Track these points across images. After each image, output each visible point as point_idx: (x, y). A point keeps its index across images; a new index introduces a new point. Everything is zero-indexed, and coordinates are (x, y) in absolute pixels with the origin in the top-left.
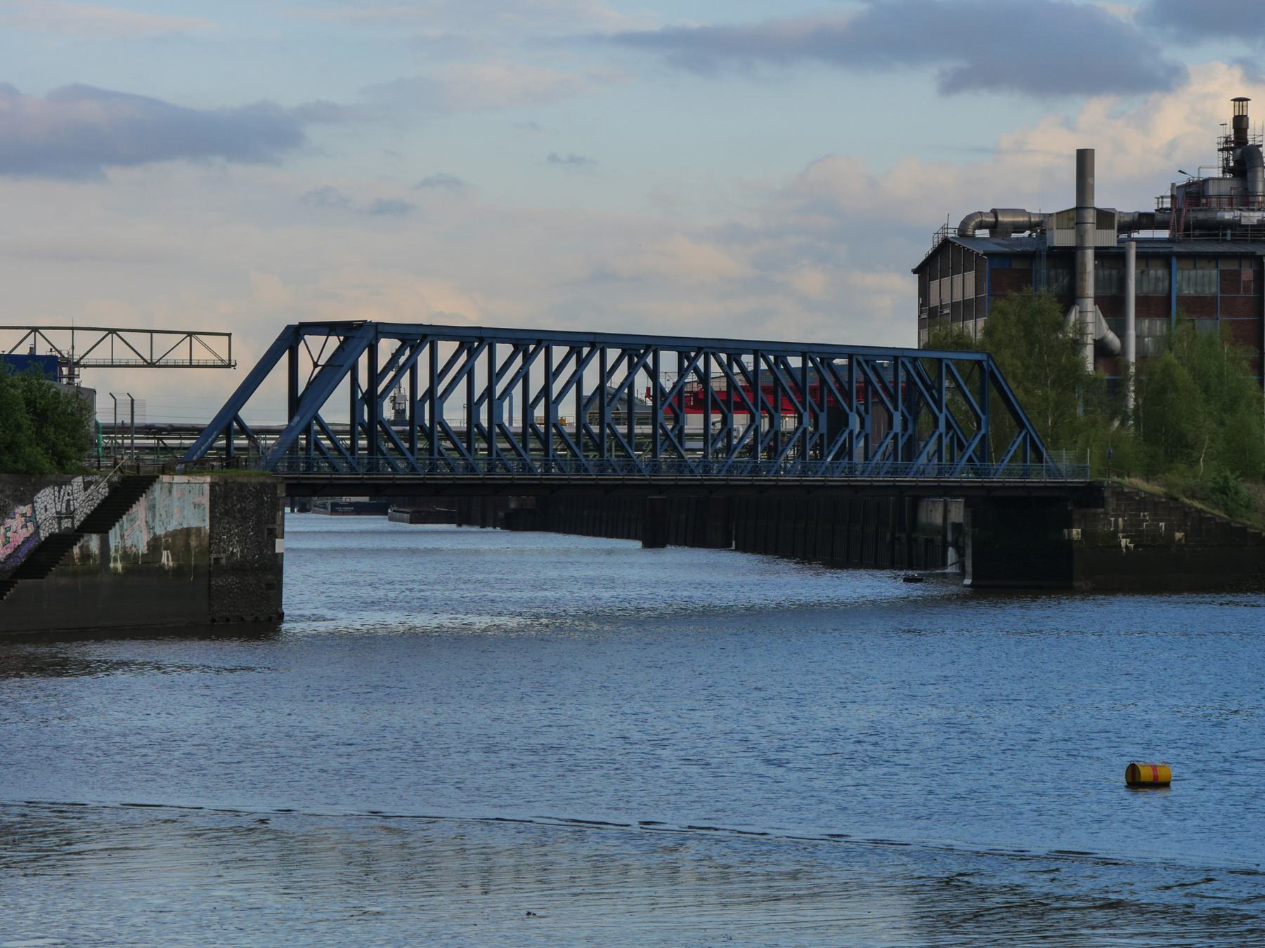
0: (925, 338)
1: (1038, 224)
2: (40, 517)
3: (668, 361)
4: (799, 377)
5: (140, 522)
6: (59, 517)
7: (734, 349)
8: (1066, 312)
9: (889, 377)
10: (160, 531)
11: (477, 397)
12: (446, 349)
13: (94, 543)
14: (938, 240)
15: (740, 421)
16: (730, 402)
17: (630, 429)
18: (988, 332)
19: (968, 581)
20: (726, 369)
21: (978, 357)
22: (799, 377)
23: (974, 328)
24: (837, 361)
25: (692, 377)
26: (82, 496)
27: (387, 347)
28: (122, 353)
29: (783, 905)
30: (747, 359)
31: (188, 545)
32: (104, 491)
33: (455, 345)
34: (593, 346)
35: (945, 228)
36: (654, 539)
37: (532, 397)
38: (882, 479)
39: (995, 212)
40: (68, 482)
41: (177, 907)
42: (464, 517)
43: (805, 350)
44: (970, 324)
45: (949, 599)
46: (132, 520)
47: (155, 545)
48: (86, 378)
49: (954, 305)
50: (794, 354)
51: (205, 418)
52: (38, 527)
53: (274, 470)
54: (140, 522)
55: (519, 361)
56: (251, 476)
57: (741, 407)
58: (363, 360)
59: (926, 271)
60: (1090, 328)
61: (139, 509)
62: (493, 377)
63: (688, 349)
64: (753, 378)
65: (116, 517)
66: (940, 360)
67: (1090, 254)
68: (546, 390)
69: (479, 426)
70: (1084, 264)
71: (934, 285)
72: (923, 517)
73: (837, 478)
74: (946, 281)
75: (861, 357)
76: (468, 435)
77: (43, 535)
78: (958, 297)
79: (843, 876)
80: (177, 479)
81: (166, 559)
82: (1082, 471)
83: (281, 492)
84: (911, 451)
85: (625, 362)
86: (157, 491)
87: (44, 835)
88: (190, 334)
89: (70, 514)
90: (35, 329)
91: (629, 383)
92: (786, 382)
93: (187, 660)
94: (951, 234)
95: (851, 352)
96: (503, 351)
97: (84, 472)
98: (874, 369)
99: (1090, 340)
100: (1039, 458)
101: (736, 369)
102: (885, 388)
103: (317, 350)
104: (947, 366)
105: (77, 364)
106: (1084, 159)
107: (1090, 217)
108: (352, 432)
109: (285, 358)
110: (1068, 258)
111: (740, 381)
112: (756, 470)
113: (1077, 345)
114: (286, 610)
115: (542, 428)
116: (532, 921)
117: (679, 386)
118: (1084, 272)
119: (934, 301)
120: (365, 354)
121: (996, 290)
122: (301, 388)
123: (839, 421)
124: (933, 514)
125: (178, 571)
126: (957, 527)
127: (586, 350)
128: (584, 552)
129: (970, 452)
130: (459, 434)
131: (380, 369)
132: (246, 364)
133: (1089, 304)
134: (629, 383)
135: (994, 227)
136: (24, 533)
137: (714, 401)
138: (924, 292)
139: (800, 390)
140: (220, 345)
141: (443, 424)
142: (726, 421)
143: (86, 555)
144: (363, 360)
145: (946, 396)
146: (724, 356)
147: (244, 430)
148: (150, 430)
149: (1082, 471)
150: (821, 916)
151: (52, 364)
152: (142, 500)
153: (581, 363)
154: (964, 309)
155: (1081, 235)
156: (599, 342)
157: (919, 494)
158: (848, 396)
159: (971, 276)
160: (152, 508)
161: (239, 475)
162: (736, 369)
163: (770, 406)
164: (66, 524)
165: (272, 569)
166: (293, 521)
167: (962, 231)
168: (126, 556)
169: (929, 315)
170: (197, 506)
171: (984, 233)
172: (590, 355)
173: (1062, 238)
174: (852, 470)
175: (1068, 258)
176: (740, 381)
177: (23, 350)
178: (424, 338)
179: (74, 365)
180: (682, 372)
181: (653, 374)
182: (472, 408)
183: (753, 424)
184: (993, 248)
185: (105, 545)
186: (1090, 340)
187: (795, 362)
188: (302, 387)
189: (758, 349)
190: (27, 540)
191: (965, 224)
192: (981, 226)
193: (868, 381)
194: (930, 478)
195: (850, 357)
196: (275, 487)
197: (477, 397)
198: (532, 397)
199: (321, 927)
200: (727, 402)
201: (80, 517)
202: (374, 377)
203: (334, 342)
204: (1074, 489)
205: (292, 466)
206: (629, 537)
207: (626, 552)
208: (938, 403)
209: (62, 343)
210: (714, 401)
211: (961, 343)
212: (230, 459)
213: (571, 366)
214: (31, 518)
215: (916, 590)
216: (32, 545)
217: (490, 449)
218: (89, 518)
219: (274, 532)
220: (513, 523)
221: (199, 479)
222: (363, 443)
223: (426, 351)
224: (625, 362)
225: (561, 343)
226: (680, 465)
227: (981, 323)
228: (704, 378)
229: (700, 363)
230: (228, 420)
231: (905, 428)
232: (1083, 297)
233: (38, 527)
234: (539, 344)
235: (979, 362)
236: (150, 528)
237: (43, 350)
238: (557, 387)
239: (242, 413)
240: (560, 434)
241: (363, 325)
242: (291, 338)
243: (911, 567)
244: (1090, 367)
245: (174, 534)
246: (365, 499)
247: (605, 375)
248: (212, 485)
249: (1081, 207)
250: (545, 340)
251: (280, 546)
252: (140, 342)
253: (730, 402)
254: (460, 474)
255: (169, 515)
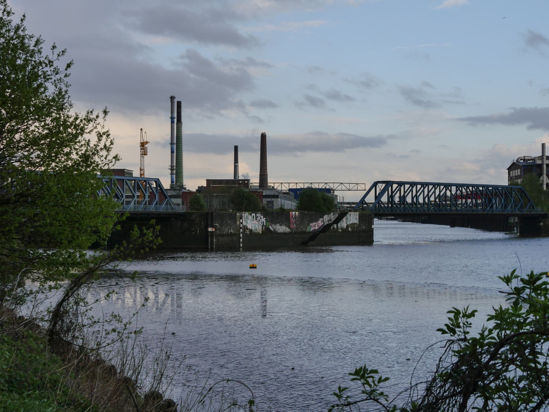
0: (509, 183)
1: (534, 159)
2: (325, 221)
3: (454, 188)
4: (491, 191)
5: (345, 222)
6: (328, 220)
7: (468, 186)
8: (540, 177)
9: (501, 191)
10: (348, 224)
11: (413, 196)
12: (407, 186)
13: (335, 226)
14: (512, 163)
15: (469, 201)
16: (467, 197)
17: (446, 203)
18: (523, 182)
19: (518, 234)
20: (466, 190)
21: (520, 187)
22: (491, 191)
23: (519, 181)
24: (490, 188)
25: (459, 192)
26: (333, 217)
27: (395, 186)
28: (344, 188)
29: (469, 300)
30: (471, 188)
31: (354, 226)
32: (337, 215)
33: (409, 185)
34: (438, 186)
35: (514, 160)
36: (453, 225)
37: (425, 196)
38: (500, 213)
39: (524, 157)
40: (330, 214)
41: (344, 299)
42: (413, 221)
43: (483, 186)
44: (519, 180)
45: (509, 239)
46: (343, 221)
47: (347, 226)
48: (336, 193)
49: (516, 176)
50: (481, 187)
51: (358, 201)
52: (324, 223)
53: (372, 211)
54: (345, 222)
55: (422, 188)
56: (367, 212)
57: (469, 198)
58: (390, 189)
59: (510, 169)
60: (545, 181)
61: (344, 219)
62: (417, 192)
63: (458, 186)
64: (472, 192)
65: (340, 221)
66: (512, 188)
67: (545, 165)
68: (428, 195)
69: (414, 202)
70: (544, 167)
71: (511, 172)
72: (509, 221)
73: (490, 213)
74: (514, 171)
75: (495, 187)
76: (412, 204)
77: (325, 224)
78: (516, 175)
79: (483, 295)
80: (352, 213)
81: (350, 229)
82: (543, 211)
83: (373, 215)
84: (506, 207)
85: (445, 188)
86: (348, 215)
87: (320, 284)
88: (357, 184)
89: (331, 220)
90: (326, 183)
91: (445, 193)
92: (479, 193)
93: (351, 250)
94: (515, 161)
95: (492, 186)
96: (442, 187)
97: (333, 212)
98: (498, 190)
99: (545, 183)
100: (533, 208)
101: (468, 190)
102: (500, 194)
103: (381, 187)
104: (126, 181)
105: (334, 190)
106: (543, 145)
107: (545, 157)
108: (388, 204)
109: (374, 188)
110: (540, 166)
111: (470, 193)
112: (473, 211)
113: (542, 184)
114: (374, 240)
115: (438, 203)
116: (416, 303)
117: (456, 193)
118: (544, 169)
119: (511, 175)
120: (390, 187)
121: (524, 173)
122: (377, 195)
123: (490, 201)
124: (511, 220)
125: (352, 232)
126: (517, 223)
127: (436, 186)
128: (434, 228)
129: (518, 207)
130: (410, 204)
131: (393, 190)
132: (367, 189)
133: (545, 176)
134: (445, 193)
135: (524, 160)
136: (321, 224)
137: (464, 197)
138: (509, 174)
139: (482, 194)
140: (363, 186)
141: (419, 202)
142: (466, 201)
143: (334, 228)
144: (390, 189)
145: (513, 195)
146: (465, 187)
147: (366, 203)
148: (348, 203)
149: (543, 211)
150: (477, 303)
151: (329, 190)
152: (345, 217)
153: (435, 189)
154: (517, 177)
155: (543, 161)
156: (439, 185)
157: (508, 216)
158: (492, 195)
159: (519, 170)
160: (347, 219)
161: (364, 212)
162: (468, 190)
163: (475, 197)
164: (330, 222)
165: (372, 231)
166: (376, 221)
167: (517, 161)
168: (342, 228)
169: (510, 178)
170: (356, 218)
171: (522, 161)
172: (437, 187)
173: (539, 162)
174: (493, 211)
175: (540, 166)
176: (470, 193)
177: (324, 187)
178: (402, 184)
179: (334, 190)
180: (457, 191)
181: (451, 191)
182: (413, 198)
183: (472, 201)
184: (524, 164)
185: (337, 226)
186: (545, 183)
187: (481, 188)
188: (377, 195)
189: (473, 186)
190: (322, 225)
191: (518, 159)
192: (521, 160)
193: (496, 192)
194: (510, 212)
195: (502, 188)
196: (372, 215)
197: (413, 196)
198: (425, 196)
199: (373, 303)
200: (466, 197)
201: (332, 221)
202: (392, 192)
203: (384, 185)
204: (542, 215)
205: (376, 210)
206: (447, 225)
207: (448, 228)
208: (512, 197)
209: (331, 186)
210: (464, 197)
211: (517, 184)
212: (363, 209)
213: (433, 189)
214: (323, 221)
215: (507, 236)
216: (323, 226)
217: (428, 207)
218: (334, 221)
219: (372, 223)
220: (424, 222)
221: (357, 213)
222: (390, 206)
223: (415, 187)
224: (445, 188)
225: (442, 185)
226: (457, 210)
227: (521, 180)
228: (461, 192)
229: (460, 189)
230: (363, 201)
231: (504, 202)
232: (544, 174)
233: (324, 223)
234: (426, 185)
235: (520, 188)
236: (347, 223)
237: (328, 187)
238: (430, 194)
239: (365, 200)
240: (431, 204)
241: (390, 181)
242: (375, 184)
243: (507, 231)
244: (545, 189)
245: (351, 224)
246: (393, 217)
247: (440, 192)
248: (359, 214)
249: (543, 155)
250: (428, 184)
251: (373, 226)
252: (347, 185)
253: (467, 197)
254: (410, 212)
255: (350, 220)
